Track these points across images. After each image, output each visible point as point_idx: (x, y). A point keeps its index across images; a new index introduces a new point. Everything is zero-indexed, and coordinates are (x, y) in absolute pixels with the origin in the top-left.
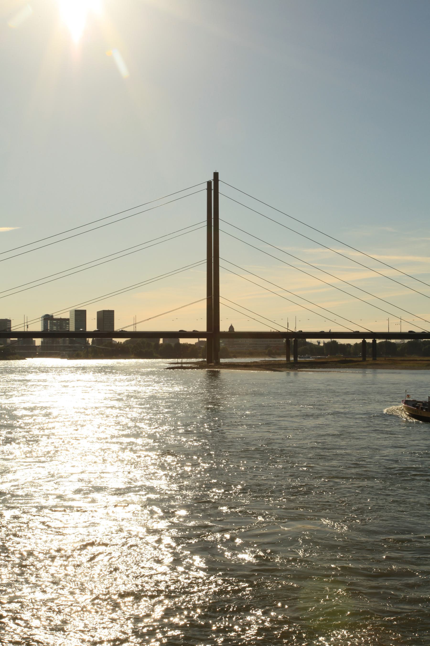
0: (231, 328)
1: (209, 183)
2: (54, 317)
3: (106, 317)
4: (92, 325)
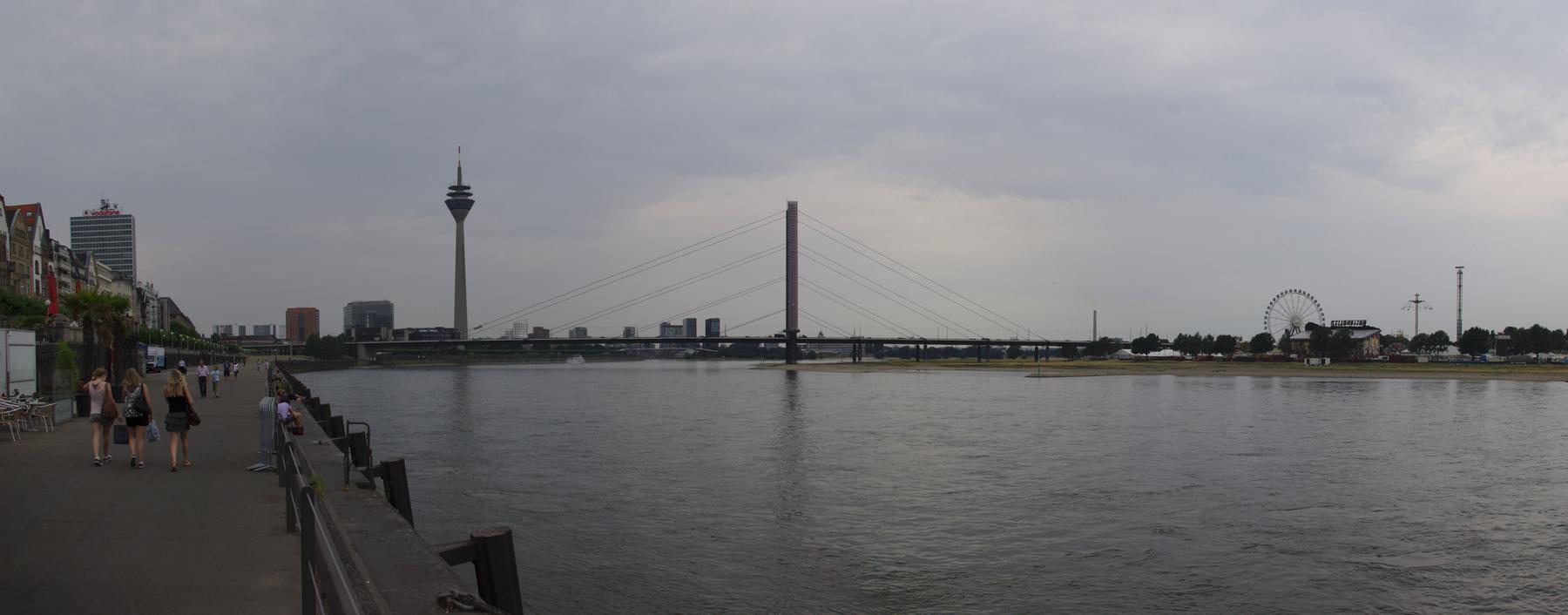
3: (712, 324)
4: (701, 332)
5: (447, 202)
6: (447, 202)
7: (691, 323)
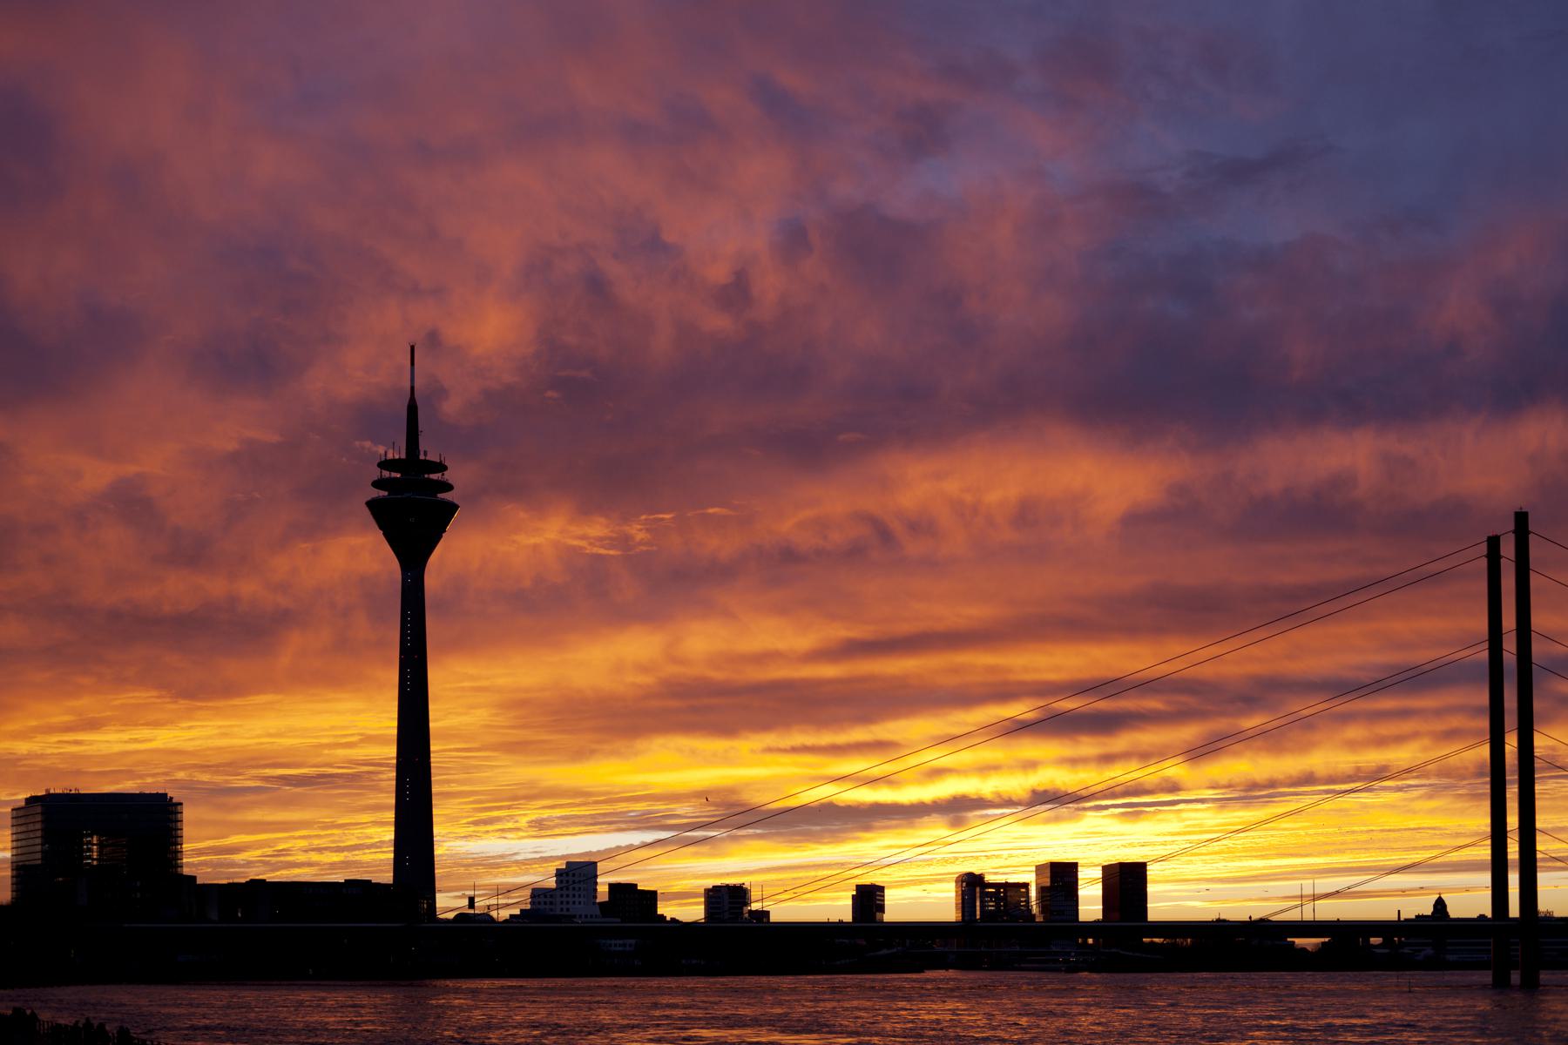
1: (1494, 543)
2: (989, 878)
4: (1090, 902)
5: (373, 505)
7: (1062, 876)
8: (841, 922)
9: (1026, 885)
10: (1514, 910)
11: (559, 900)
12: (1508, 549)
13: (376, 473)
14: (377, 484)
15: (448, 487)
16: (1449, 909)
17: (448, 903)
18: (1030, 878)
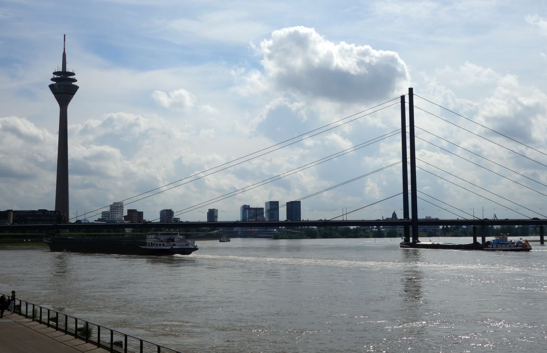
0: (212, 213)
1: (403, 98)
4: (283, 216)
5: (51, 87)
6: (51, 87)
7: (274, 206)
8: (44, 211)
9: (263, 209)
10: (410, 216)
11: (111, 215)
12: (407, 100)
13: (52, 76)
14: (53, 80)
15: (75, 80)
16: (397, 216)
17: (72, 219)
18: (263, 206)
